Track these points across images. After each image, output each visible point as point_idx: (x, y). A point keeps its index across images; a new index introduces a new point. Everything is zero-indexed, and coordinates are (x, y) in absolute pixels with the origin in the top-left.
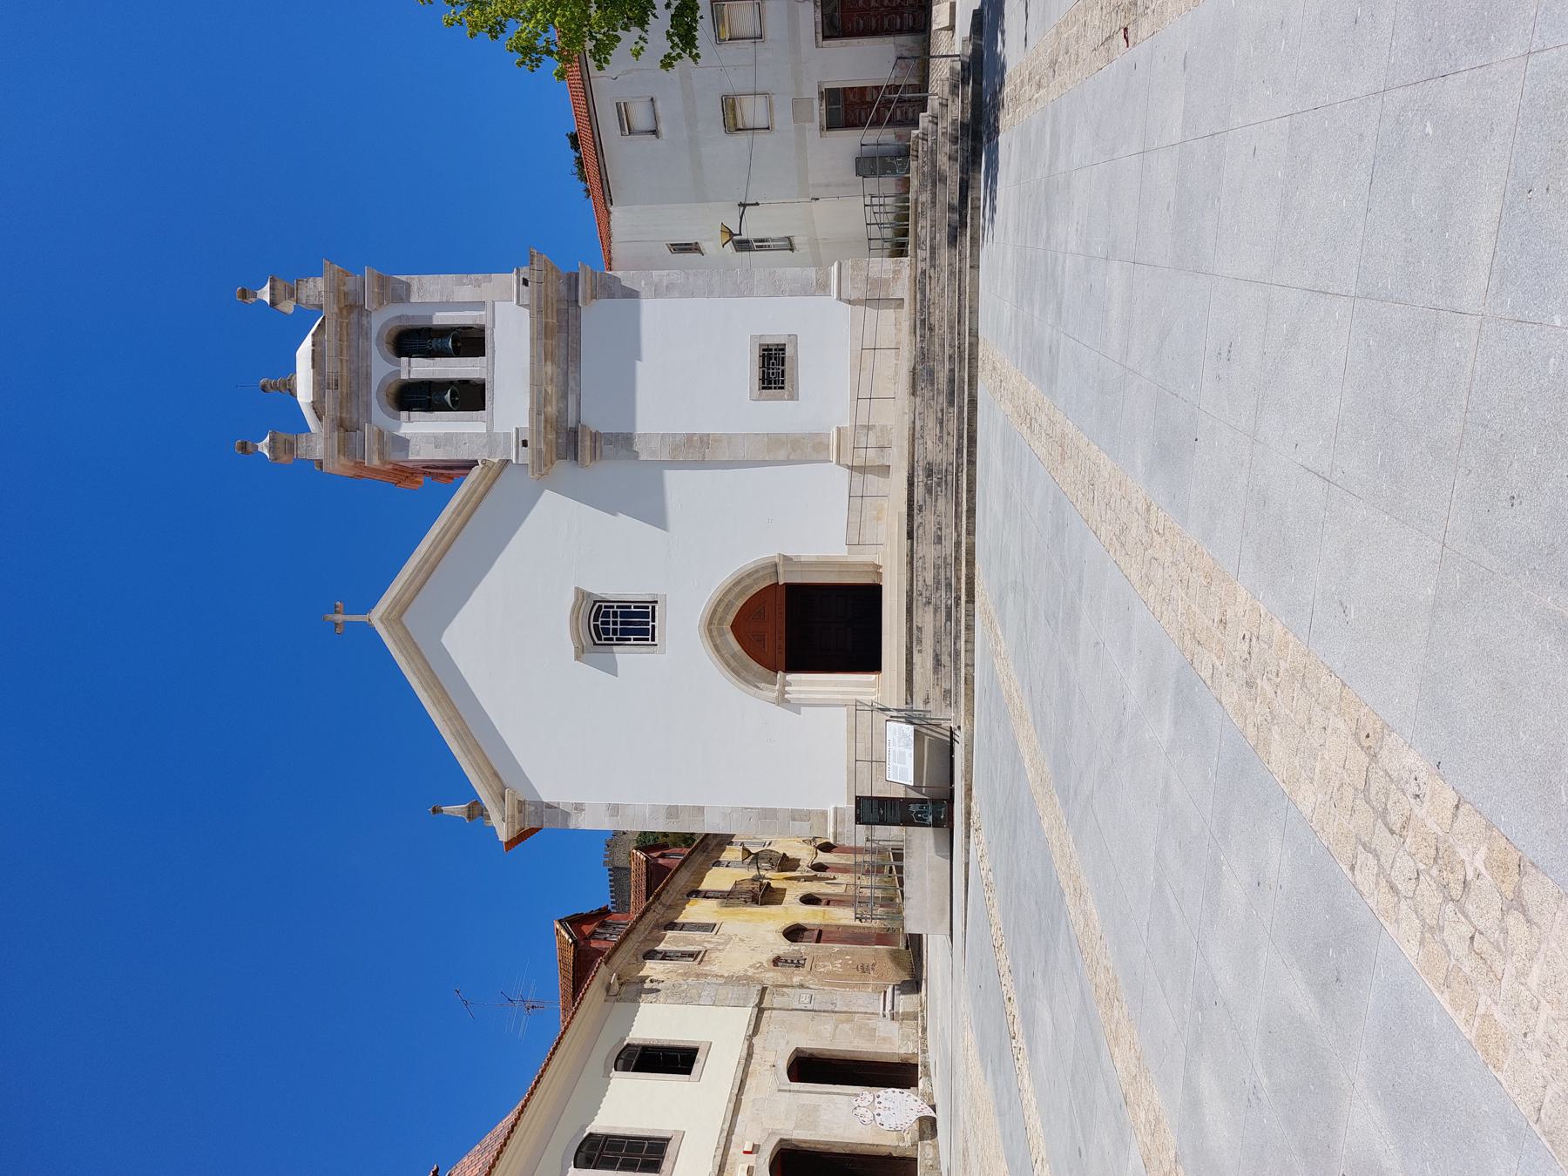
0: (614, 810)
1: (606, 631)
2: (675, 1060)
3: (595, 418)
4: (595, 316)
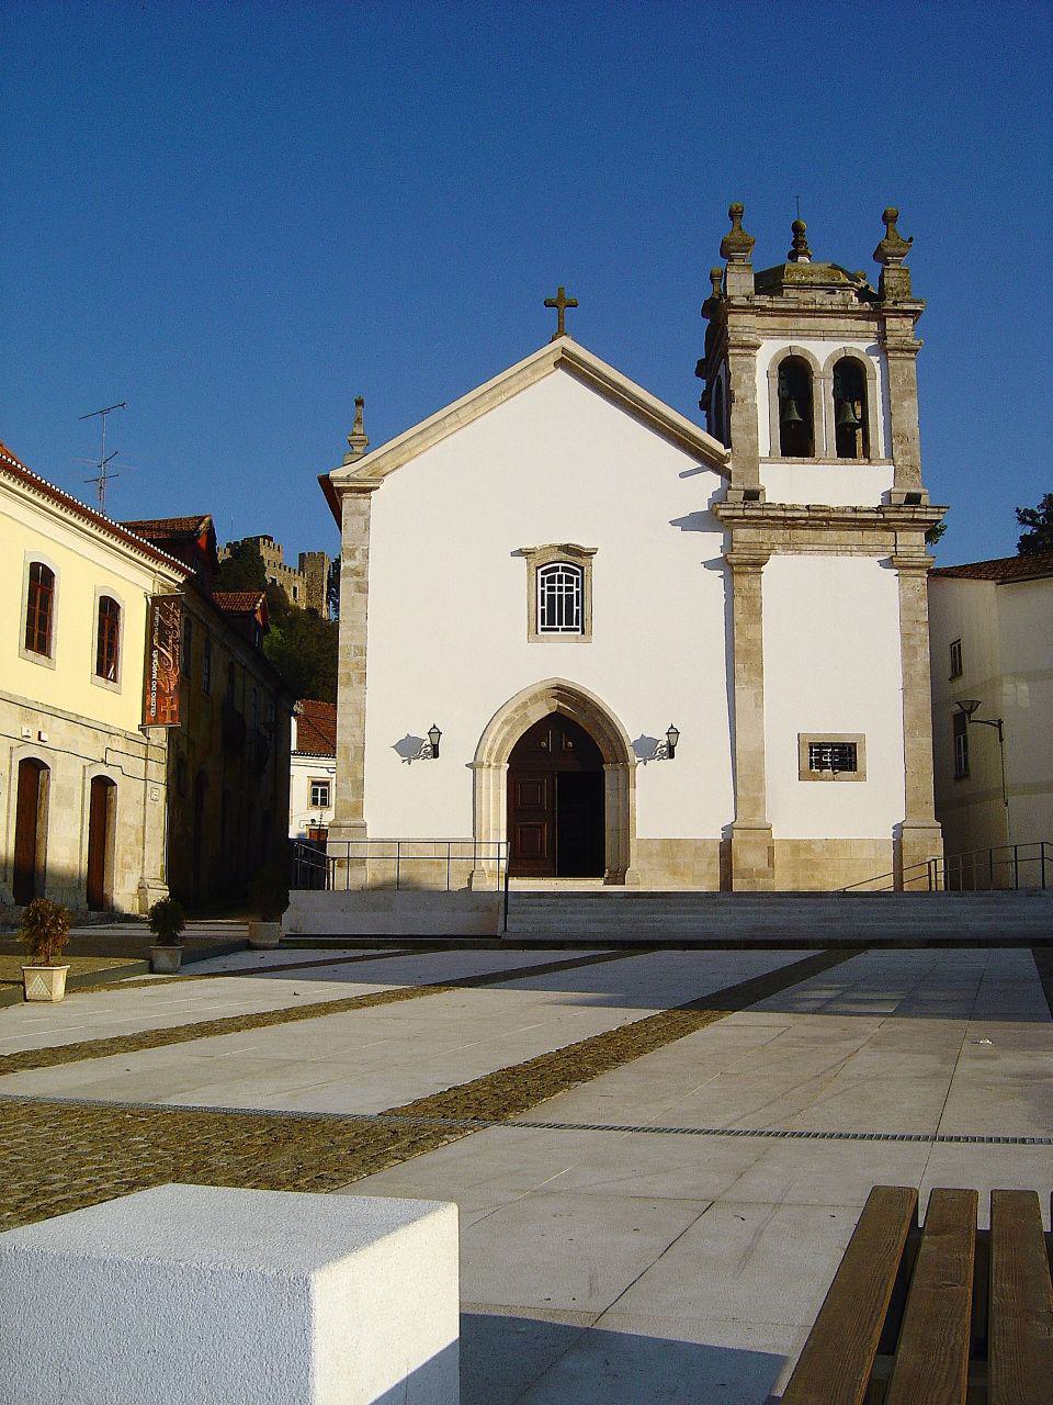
1: (551, 580)
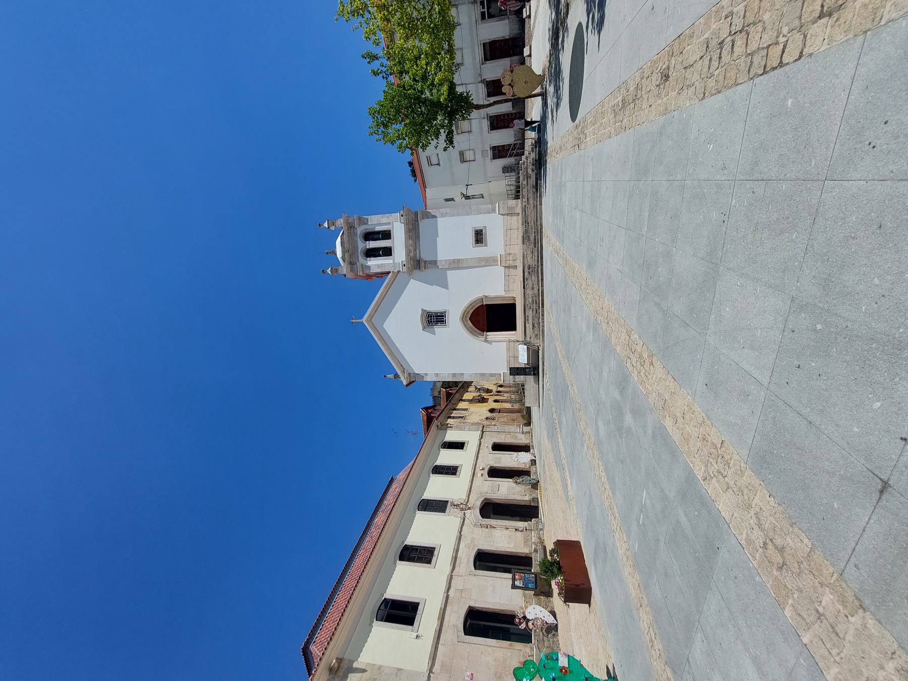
0: (437, 375)
2: (459, 446)
3: (425, 256)
4: (423, 224)
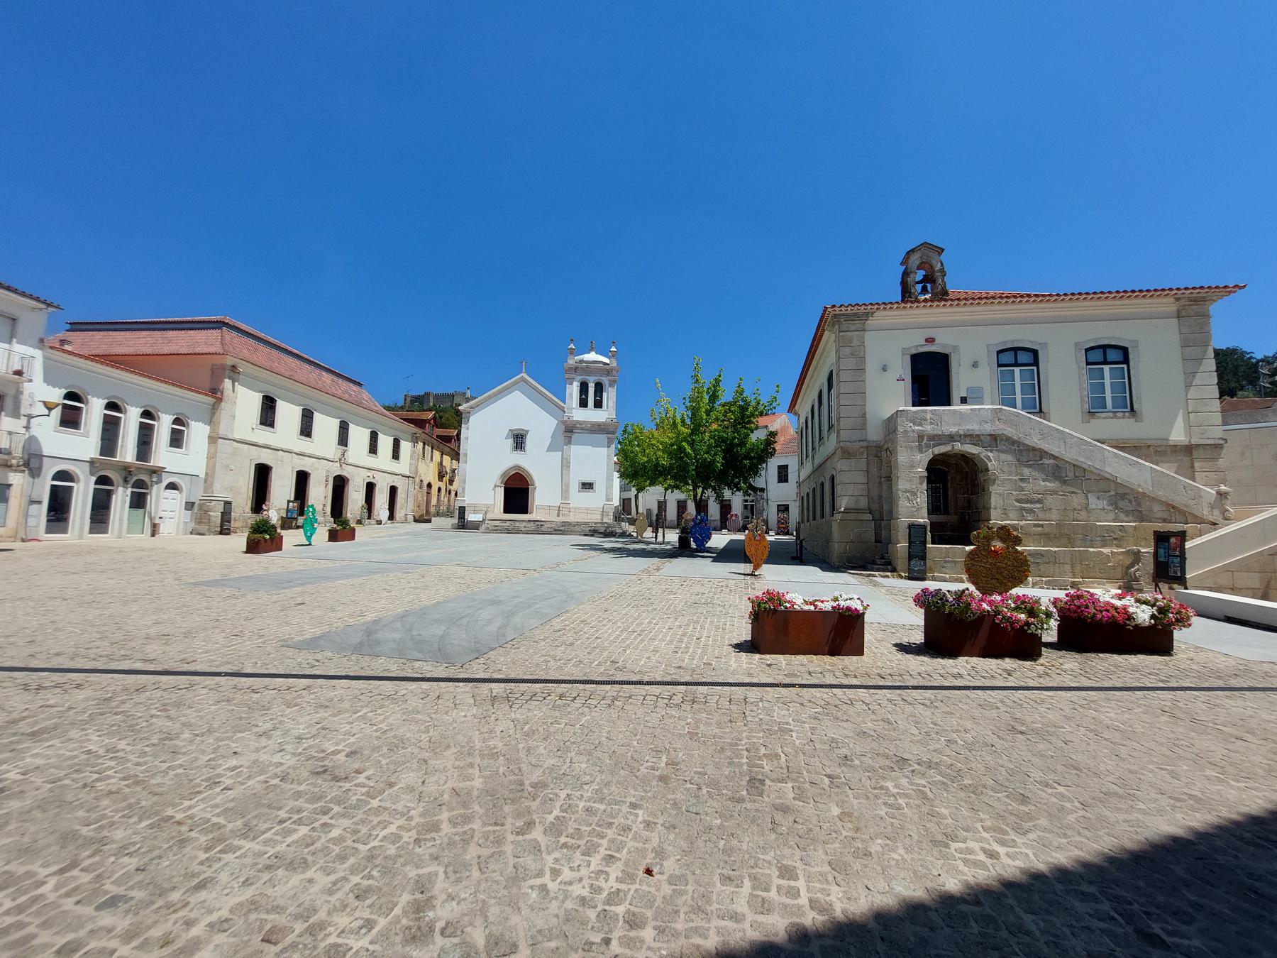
2: (396, 455)
3: (575, 436)
4: (604, 438)
